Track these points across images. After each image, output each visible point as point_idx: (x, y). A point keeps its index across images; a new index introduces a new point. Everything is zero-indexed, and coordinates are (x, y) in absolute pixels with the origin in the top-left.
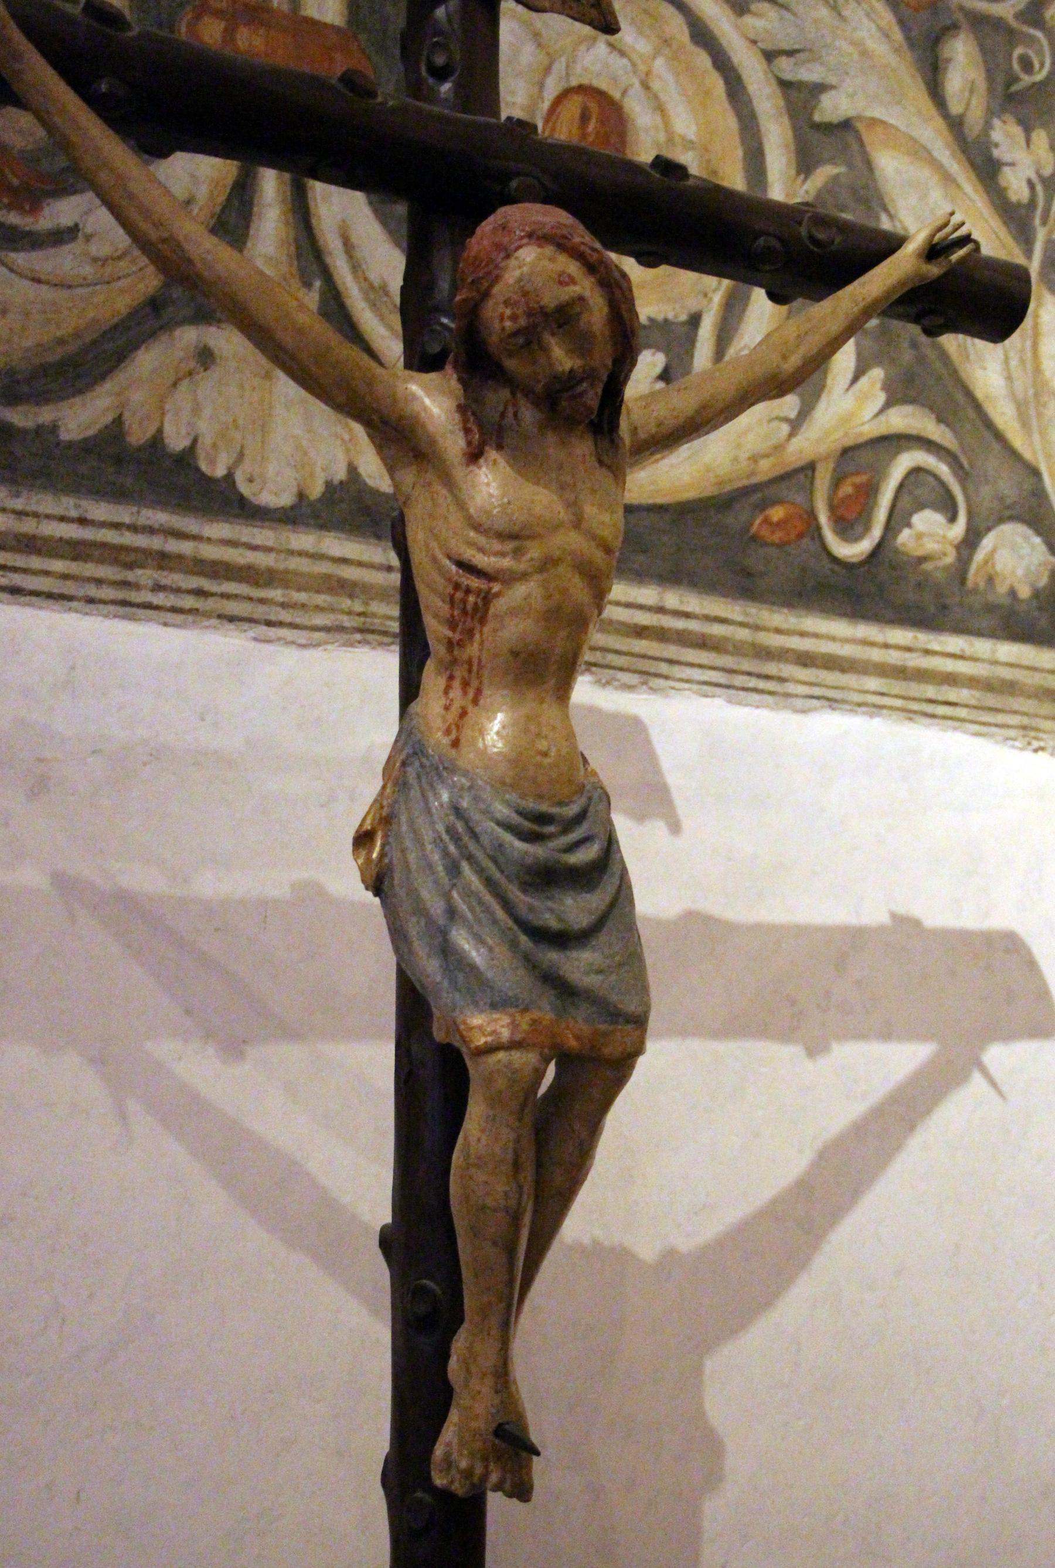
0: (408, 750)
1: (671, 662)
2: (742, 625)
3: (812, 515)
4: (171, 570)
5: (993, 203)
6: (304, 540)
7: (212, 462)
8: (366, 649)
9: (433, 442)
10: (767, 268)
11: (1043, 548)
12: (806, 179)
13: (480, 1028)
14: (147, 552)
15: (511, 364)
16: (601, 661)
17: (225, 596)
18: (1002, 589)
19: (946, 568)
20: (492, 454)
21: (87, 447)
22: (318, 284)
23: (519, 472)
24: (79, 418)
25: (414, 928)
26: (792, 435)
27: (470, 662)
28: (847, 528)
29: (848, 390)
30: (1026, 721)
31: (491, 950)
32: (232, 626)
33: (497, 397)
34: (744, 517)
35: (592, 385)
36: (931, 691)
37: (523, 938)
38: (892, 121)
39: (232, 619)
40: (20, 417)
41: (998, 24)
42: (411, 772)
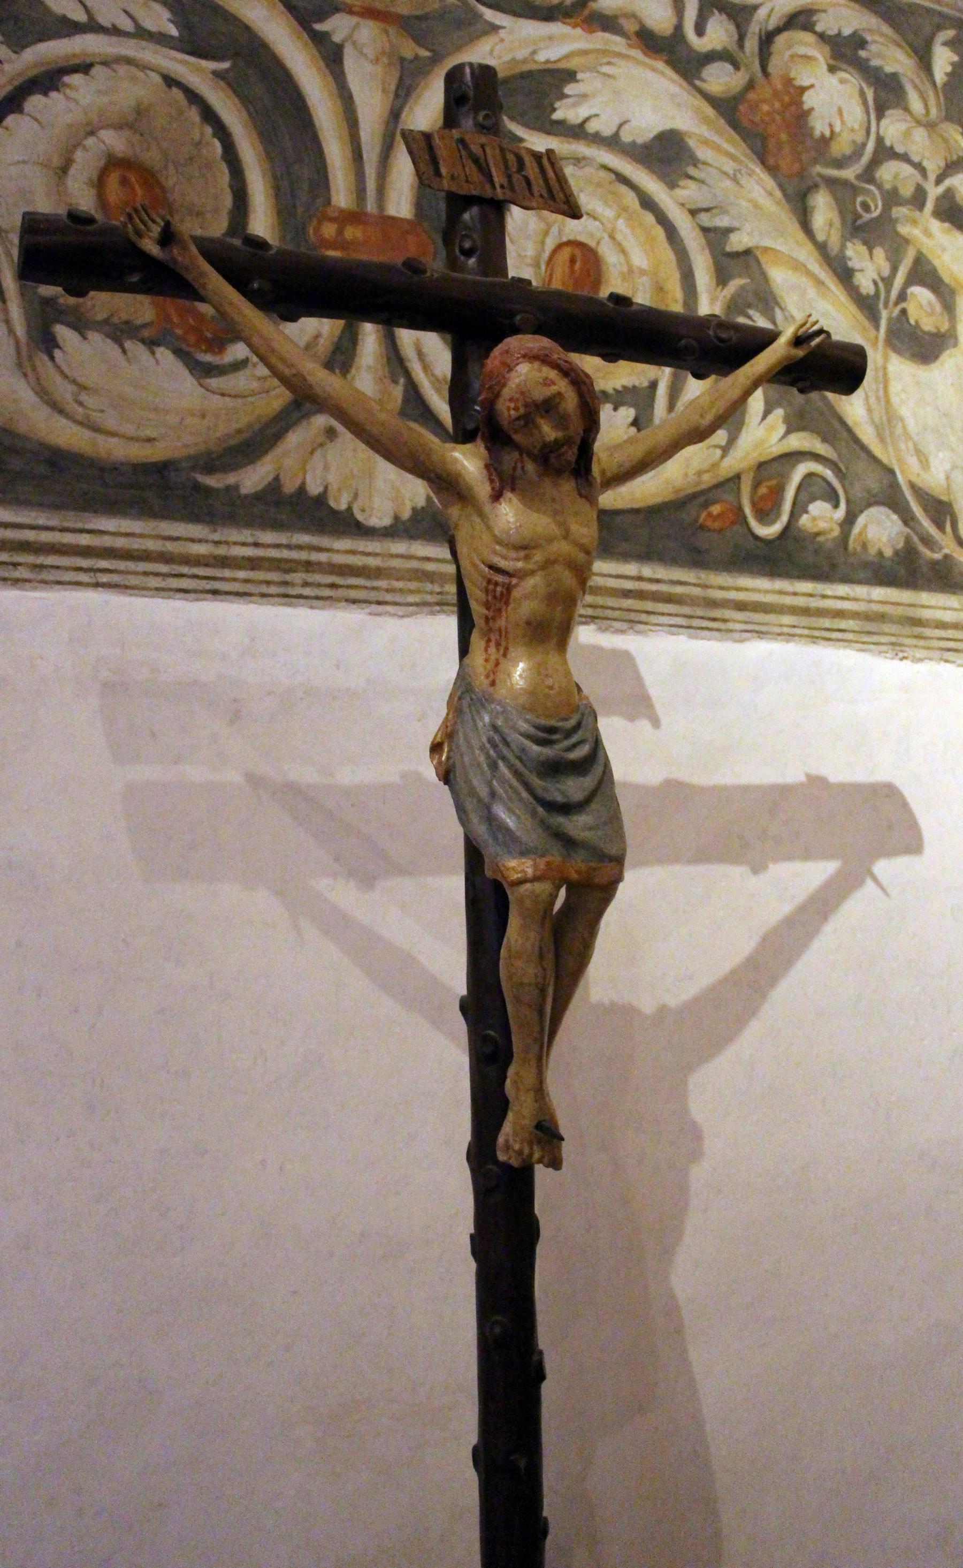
0: (463, 689)
1: (648, 613)
2: (695, 585)
3: (740, 509)
4: (313, 572)
5: (850, 296)
6: (399, 547)
7: (337, 500)
8: (443, 616)
9: (470, 489)
10: (688, 358)
11: (900, 523)
12: (723, 288)
13: (513, 868)
14: (297, 562)
15: (517, 437)
16: (601, 615)
17: (349, 587)
18: (872, 551)
19: (834, 540)
20: (508, 495)
21: (258, 497)
22: (402, 381)
23: (525, 505)
24: (252, 479)
25: (470, 805)
26: (723, 457)
27: (500, 631)
28: (764, 515)
29: (760, 424)
30: (893, 639)
31: (518, 818)
32: (355, 606)
33: (510, 458)
34: (694, 513)
35: (570, 448)
36: (827, 623)
37: (540, 809)
38: (779, 248)
39: (354, 602)
40: (212, 481)
41: (845, 183)
42: (465, 703)
